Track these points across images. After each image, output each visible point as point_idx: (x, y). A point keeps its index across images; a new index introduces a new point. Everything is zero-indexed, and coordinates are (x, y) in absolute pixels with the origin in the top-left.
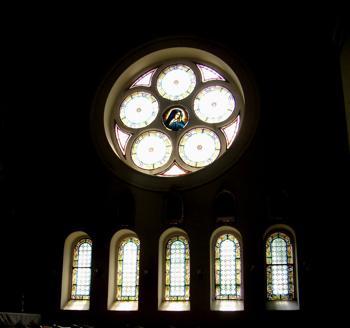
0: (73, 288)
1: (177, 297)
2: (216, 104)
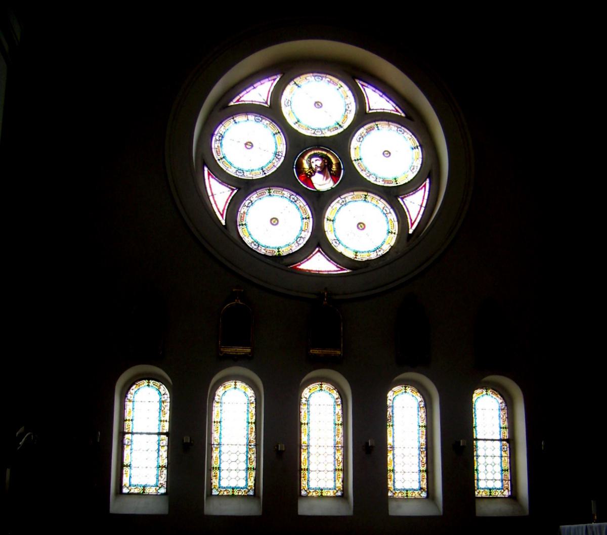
0: (213, 473)
1: (233, 489)
2: (390, 153)
